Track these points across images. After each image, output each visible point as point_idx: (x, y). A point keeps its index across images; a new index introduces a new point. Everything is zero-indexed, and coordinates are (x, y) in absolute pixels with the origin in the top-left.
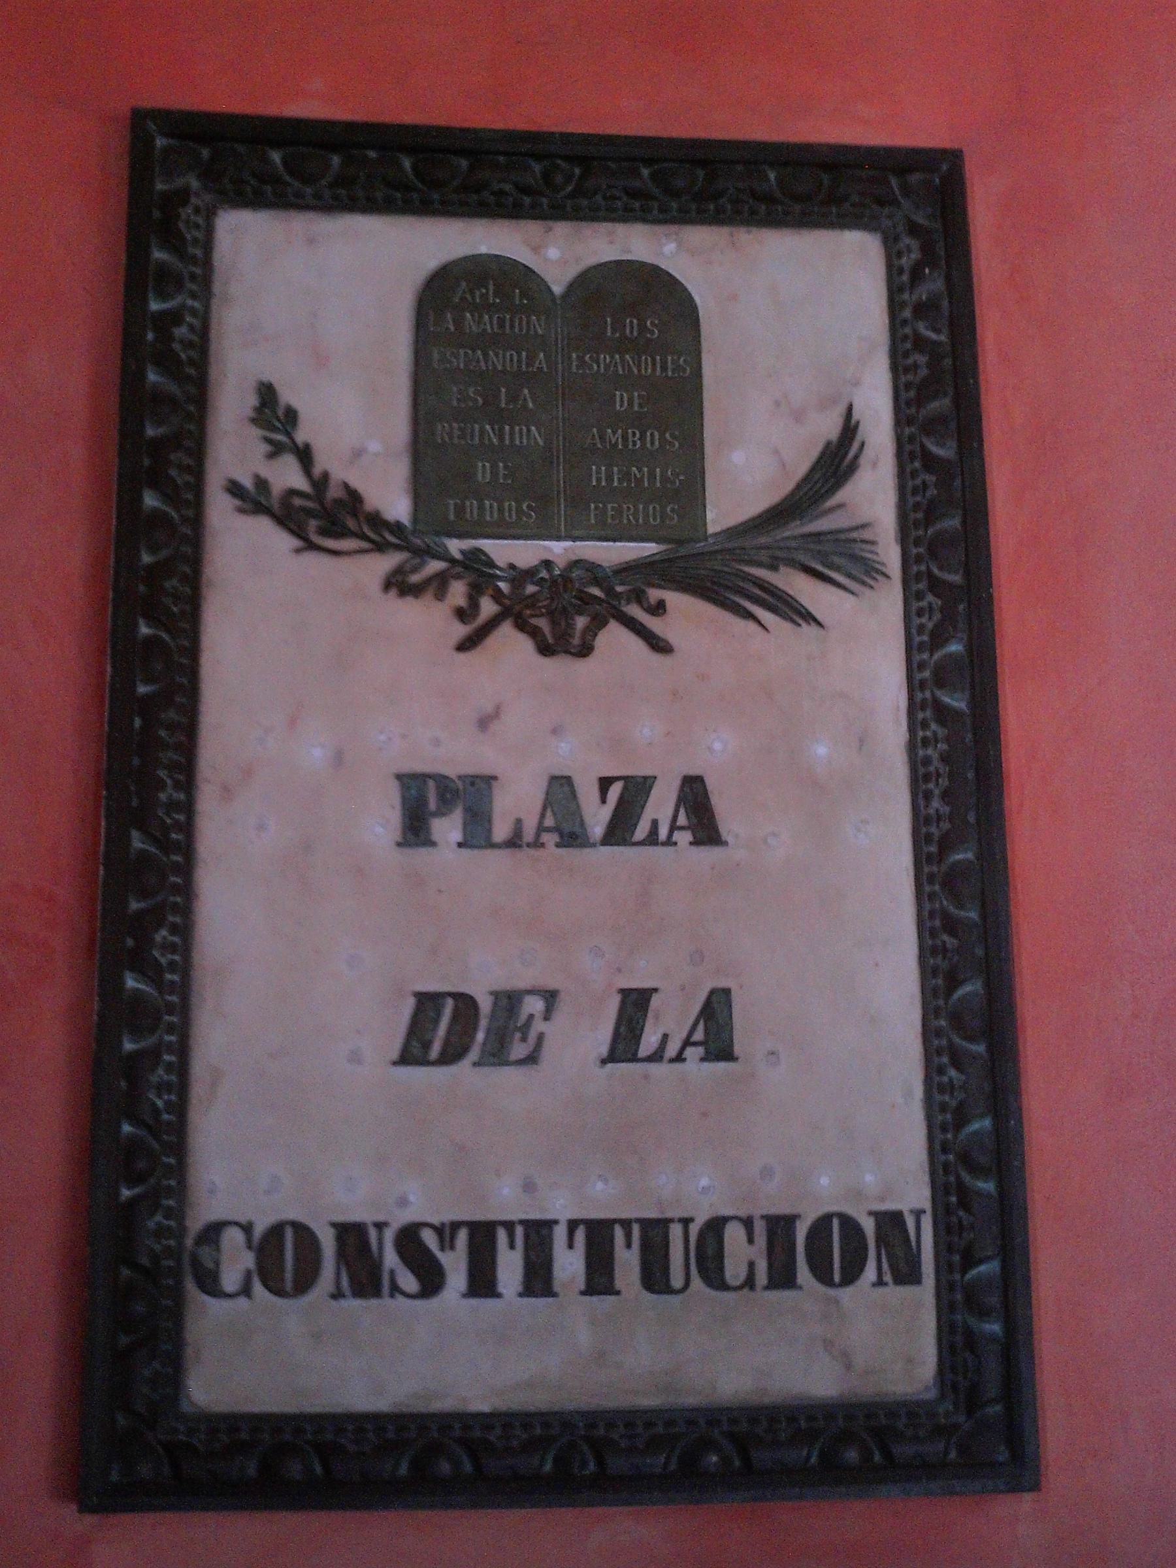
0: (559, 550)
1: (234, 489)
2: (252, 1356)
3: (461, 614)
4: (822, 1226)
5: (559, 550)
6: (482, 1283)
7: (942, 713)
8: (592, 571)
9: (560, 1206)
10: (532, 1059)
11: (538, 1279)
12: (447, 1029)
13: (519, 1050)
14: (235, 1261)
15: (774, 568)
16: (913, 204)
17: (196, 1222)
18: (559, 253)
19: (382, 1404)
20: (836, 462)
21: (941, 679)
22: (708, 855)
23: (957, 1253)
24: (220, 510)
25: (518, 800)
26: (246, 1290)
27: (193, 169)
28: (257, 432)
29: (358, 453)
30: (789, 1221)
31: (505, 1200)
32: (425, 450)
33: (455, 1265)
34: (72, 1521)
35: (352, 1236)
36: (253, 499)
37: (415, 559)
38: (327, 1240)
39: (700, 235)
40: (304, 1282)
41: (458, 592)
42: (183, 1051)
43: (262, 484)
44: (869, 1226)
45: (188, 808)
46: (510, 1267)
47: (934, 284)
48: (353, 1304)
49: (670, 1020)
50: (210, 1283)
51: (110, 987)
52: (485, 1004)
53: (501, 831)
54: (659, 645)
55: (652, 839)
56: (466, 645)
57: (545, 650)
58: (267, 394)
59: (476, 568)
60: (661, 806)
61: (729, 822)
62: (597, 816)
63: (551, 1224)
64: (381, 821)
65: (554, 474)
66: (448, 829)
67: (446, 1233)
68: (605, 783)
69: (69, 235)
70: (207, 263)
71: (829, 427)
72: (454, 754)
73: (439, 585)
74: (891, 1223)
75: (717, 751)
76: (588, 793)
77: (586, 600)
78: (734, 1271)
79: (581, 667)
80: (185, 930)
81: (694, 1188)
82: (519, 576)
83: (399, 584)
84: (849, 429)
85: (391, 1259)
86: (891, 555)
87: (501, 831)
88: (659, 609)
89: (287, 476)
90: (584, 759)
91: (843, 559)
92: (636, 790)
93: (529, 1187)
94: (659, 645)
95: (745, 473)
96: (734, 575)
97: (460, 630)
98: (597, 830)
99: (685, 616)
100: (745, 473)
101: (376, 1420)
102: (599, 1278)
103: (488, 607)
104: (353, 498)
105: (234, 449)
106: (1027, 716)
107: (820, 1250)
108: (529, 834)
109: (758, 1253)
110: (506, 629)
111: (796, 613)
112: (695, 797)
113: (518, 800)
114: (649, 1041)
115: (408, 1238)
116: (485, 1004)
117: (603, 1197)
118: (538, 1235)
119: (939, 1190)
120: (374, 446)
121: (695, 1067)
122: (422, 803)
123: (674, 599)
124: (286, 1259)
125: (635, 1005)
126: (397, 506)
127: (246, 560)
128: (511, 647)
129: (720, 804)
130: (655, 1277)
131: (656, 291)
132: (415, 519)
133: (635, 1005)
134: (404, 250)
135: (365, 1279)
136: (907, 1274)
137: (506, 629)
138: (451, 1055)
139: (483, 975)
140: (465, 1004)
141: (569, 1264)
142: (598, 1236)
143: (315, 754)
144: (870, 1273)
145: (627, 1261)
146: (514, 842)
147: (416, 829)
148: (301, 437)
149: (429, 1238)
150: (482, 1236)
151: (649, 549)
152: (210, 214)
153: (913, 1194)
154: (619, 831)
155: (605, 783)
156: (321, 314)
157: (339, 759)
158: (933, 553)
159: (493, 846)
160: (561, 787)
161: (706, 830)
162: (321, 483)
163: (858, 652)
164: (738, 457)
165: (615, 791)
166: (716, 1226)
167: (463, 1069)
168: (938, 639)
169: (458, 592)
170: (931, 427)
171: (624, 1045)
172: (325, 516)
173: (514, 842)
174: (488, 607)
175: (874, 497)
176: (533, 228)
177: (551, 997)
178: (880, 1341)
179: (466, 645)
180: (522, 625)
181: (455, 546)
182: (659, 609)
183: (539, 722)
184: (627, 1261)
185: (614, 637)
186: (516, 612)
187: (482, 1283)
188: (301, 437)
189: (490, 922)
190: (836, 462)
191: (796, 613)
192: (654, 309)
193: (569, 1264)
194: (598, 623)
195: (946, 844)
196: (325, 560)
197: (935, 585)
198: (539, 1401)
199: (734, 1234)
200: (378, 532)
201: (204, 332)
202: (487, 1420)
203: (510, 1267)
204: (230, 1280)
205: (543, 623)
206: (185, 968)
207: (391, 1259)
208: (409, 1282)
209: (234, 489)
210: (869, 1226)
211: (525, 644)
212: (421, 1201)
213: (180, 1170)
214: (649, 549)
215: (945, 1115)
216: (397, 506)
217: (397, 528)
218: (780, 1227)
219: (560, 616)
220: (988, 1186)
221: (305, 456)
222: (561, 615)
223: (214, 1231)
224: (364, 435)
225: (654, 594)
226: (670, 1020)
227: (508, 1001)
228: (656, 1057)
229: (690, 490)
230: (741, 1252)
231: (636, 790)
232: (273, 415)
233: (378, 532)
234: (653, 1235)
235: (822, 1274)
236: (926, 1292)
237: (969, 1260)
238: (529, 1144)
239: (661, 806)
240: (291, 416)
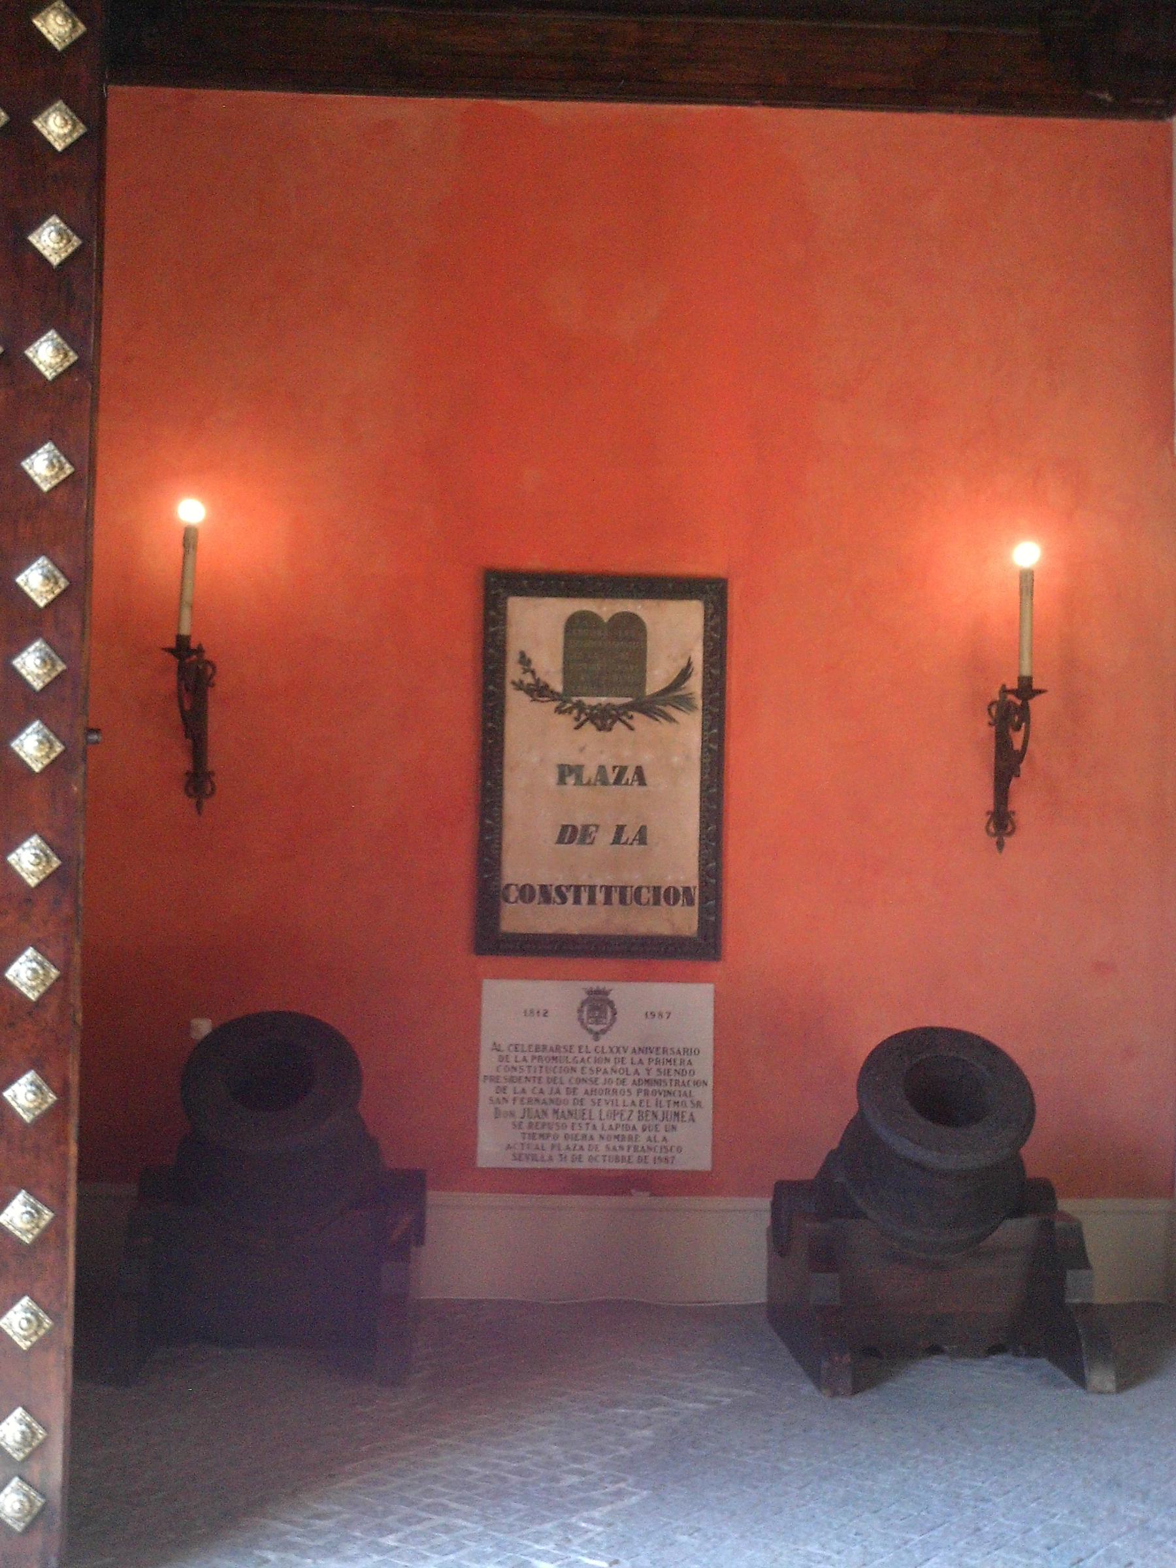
0: (603, 700)
1: (513, 683)
2: (517, 918)
3: (577, 719)
4: (668, 890)
5: (603, 700)
6: (577, 901)
7: (710, 750)
8: (613, 707)
9: (599, 881)
10: (592, 843)
11: (592, 900)
12: (569, 834)
13: (588, 841)
14: (513, 894)
15: (665, 705)
16: (711, 592)
17: (505, 882)
18: (605, 609)
19: (550, 931)
20: (685, 674)
21: (710, 741)
22: (643, 788)
23: (704, 899)
24: (510, 690)
25: (590, 772)
26: (516, 902)
27: (502, 585)
28: (520, 666)
29: (547, 673)
30: (659, 888)
31: (584, 879)
32: (566, 670)
33: (570, 896)
34: (474, 957)
35: (543, 888)
36: (519, 686)
37: (563, 702)
38: (537, 888)
39: (649, 603)
40: (531, 899)
41: (575, 712)
42: (500, 839)
43: (521, 682)
44: (681, 890)
45: (501, 774)
46: (585, 897)
47: (717, 620)
48: (543, 906)
49: (630, 834)
50: (507, 900)
51: (482, 823)
52: (580, 828)
53: (585, 781)
54: (631, 728)
55: (627, 784)
56: (577, 728)
57: (600, 729)
58: (523, 655)
59: (580, 706)
60: (630, 774)
61: (649, 780)
62: (612, 778)
63: (595, 886)
64: (552, 779)
65: (605, 679)
66: (571, 780)
67: (568, 888)
68: (614, 767)
69: (465, 603)
70: (505, 615)
71: (683, 663)
72: (572, 759)
73: (570, 711)
74: (687, 890)
75: (646, 759)
76: (609, 770)
77: (611, 716)
78: (644, 900)
79: (608, 734)
80: (501, 807)
81: (634, 878)
82: (592, 708)
83: (559, 710)
84: (689, 664)
85: (554, 894)
86: (699, 703)
87: (585, 781)
88: (631, 718)
89: (528, 679)
90: (608, 760)
91: (685, 703)
92: (623, 770)
93: (590, 877)
94: (631, 728)
95: (658, 676)
96: (651, 707)
97: (576, 724)
98: (612, 781)
99: (639, 720)
100: (658, 676)
101: (550, 935)
102: (608, 901)
103: (583, 717)
104: (546, 686)
105: (513, 671)
106: (735, 750)
107: (668, 896)
108: (593, 781)
109: (651, 895)
110: (588, 723)
111: (670, 719)
112: (639, 771)
113: (590, 772)
114: (624, 839)
115: (558, 888)
116: (580, 828)
117: (608, 879)
118: (592, 888)
119: (701, 882)
120: (552, 670)
121: (599, 786)
122: (566, 772)
123: (636, 715)
124: (526, 893)
125: (620, 829)
126: (558, 687)
127: (518, 705)
128: (589, 728)
129: (646, 773)
130: (623, 901)
131: (633, 620)
132: (564, 689)
133: (620, 829)
134: (563, 608)
135: (547, 899)
136: (690, 902)
137: (588, 723)
138: (570, 842)
139: (579, 820)
140: (574, 828)
141: (600, 896)
142: (608, 890)
143: (535, 759)
144: (681, 902)
145: (615, 897)
146: (588, 784)
147: (562, 780)
148: (532, 667)
149: (564, 889)
150: (578, 888)
151: (630, 699)
152: (506, 598)
153: (694, 882)
154: (617, 781)
155: (614, 767)
156: (538, 628)
157: (542, 760)
158: (710, 703)
159: (582, 785)
160: (602, 769)
161: (642, 781)
162: (538, 681)
163: (689, 729)
164: (656, 672)
165: (617, 770)
166: (639, 889)
167: (573, 845)
168: (710, 729)
169: (575, 712)
170: (713, 665)
171: (617, 840)
172: (539, 691)
173: (588, 784)
174: (583, 717)
175: (695, 685)
176: (598, 601)
177: (597, 826)
178: (684, 920)
179: (577, 728)
180: (592, 722)
181: (575, 699)
182: (631, 718)
183: (595, 749)
184: (615, 897)
185: (618, 725)
186: (591, 718)
187: (577, 901)
188: (532, 667)
189: (581, 805)
190: (685, 674)
191: (670, 719)
192: (632, 627)
193: (600, 896)
194: (614, 722)
195: (709, 787)
196: (539, 704)
197: (711, 713)
198: (591, 932)
199: (644, 890)
200: (553, 696)
201: (504, 636)
202: (577, 936)
203: (585, 897)
204: (512, 899)
205: (599, 722)
206: (501, 816)
207: (554, 894)
208: (558, 900)
209: (513, 683)
210: (681, 890)
211: (593, 727)
212: (561, 879)
213: (499, 870)
214: (630, 699)
215: (703, 862)
216: (558, 687)
217: (558, 694)
218: (657, 889)
219: (603, 719)
220: (713, 881)
221: (533, 672)
222: (603, 719)
223: (508, 886)
224: (549, 665)
225: (630, 713)
226: (630, 834)
227: (586, 828)
228: (625, 843)
229: (642, 683)
230: (646, 895)
231: (623, 770)
232: (524, 660)
233: (553, 696)
234: (623, 890)
235: (668, 903)
236: (696, 908)
237: (707, 899)
238: (589, 865)
239: (630, 774)
240: (529, 661)
